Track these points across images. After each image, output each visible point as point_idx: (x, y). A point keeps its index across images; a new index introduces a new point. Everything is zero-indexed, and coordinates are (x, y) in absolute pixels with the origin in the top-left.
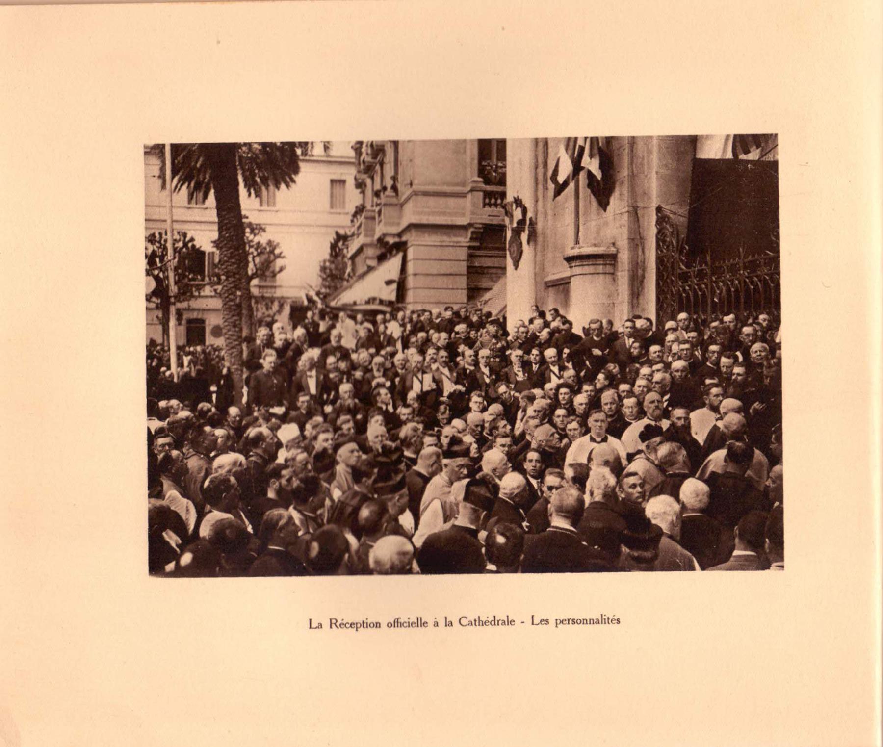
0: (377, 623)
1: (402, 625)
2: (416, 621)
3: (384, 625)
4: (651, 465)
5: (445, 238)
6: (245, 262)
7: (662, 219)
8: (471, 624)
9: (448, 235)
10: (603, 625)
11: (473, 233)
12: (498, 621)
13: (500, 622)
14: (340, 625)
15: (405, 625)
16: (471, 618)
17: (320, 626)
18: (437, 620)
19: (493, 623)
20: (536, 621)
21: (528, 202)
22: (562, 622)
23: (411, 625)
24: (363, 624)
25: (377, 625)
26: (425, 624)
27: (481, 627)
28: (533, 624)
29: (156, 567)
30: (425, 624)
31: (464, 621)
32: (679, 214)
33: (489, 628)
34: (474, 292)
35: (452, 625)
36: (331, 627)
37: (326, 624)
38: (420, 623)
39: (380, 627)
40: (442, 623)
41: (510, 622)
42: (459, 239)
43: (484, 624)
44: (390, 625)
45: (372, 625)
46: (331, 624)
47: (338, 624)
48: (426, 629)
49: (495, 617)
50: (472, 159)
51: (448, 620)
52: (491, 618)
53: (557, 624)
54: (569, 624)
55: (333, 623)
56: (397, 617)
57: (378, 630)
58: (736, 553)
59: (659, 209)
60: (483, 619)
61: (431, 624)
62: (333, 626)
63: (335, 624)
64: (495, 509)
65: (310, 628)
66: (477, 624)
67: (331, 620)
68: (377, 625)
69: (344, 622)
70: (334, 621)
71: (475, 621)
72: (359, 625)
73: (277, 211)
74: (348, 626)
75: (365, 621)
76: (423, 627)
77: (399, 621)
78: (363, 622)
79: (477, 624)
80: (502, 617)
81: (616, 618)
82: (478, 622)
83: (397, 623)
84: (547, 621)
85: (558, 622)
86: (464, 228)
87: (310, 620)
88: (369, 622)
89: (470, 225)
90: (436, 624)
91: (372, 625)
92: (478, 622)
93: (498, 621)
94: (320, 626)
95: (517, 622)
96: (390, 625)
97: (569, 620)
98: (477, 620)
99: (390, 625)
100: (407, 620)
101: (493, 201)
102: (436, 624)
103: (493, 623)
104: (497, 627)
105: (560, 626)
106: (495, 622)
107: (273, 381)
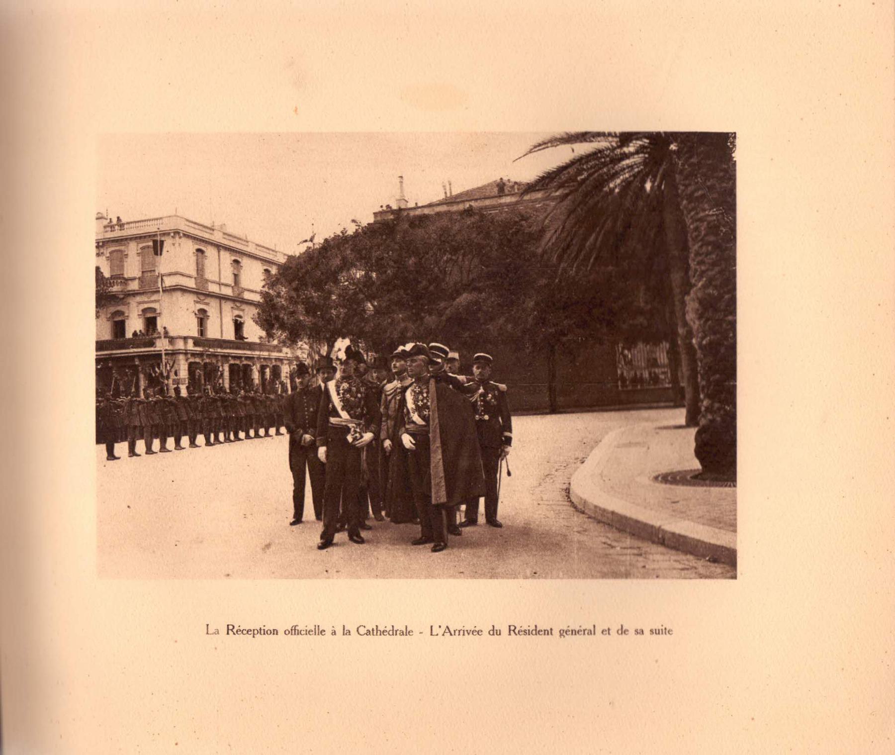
0: (575, 634)
1: (299, 633)
3: (281, 632)
8: (368, 633)
12: (396, 631)
13: (398, 632)
14: (519, 632)
15: (302, 632)
17: (217, 632)
22: (590, 633)
23: (308, 632)
24: (260, 631)
25: (275, 632)
26: (322, 632)
28: (431, 635)
29: (735, 133)
30: (322, 632)
31: (362, 631)
33: (387, 638)
36: (228, 634)
37: (505, 631)
40: (339, 631)
41: (407, 632)
43: (383, 633)
45: (269, 632)
47: (517, 631)
48: (628, 636)
49: (536, 626)
50: (647, 420)
52: (389, 628)
54: (584, 634)
55: (512, 630)
60: (381, 628)
63: (514, 631)
65: (431, 635)
66: (375, 633)
67: (510, 626)
68: (275, 632)
70: (512, 628)
71: (373, 630)
72: (256, 632)
73: (450, 184)
74: (245, 632)
77: (297, 628)
78: (260, 629)
79: (375, 633)
80: (400, 627)
82: (376, 631)
83: (294, 631)
84: (637, 632)
87: (208, 625)
90: (334, 633)
91: (269, 632)
92: (376, 631)
93: (396, 631)
94: (217, 632)
95: (416, 633)
96: (287, 632)
97: (584, 631)
98: (375, 629)
100: (527, 628)
103: (391, 633)
106: (394, 632)
107: (378, 277)
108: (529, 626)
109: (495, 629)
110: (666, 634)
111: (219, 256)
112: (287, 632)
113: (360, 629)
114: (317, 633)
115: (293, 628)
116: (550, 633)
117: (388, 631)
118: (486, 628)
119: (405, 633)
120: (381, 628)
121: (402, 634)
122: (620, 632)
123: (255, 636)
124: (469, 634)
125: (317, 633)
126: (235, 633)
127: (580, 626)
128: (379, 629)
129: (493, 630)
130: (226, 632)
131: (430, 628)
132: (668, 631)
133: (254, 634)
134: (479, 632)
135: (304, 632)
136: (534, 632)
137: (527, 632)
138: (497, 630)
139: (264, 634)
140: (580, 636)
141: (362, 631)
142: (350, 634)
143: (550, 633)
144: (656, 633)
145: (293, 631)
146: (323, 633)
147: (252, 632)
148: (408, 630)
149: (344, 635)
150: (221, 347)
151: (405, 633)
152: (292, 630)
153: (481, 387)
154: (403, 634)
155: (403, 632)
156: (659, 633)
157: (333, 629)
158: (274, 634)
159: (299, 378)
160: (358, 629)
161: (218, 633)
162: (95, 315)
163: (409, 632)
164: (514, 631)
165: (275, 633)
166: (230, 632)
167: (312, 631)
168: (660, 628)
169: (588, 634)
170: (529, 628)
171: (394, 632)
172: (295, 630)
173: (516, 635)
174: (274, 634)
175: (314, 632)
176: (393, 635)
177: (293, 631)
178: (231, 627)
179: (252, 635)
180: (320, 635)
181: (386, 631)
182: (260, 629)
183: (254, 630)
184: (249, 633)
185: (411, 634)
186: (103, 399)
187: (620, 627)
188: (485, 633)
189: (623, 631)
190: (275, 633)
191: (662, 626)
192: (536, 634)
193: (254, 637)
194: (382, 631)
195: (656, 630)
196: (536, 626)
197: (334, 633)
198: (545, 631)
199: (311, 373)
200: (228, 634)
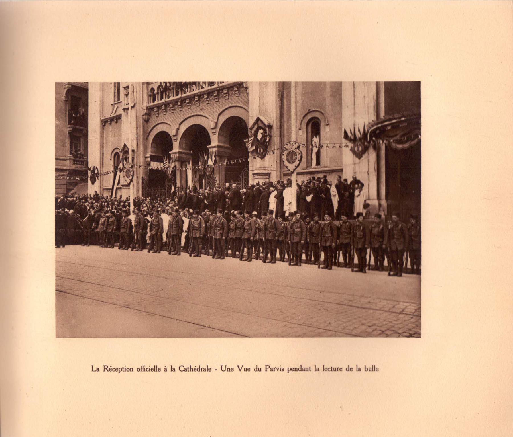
3: (135, 370)
5: (60, 173)
6: (146, 221)
7: (143, 179)
8: (186, 370)
9: (61, 172)
10: (307, 372)
11: (69, 172)
12: (202, 369)
13: (203, 369)
14: (110, 369)
15: (147, 370)
17: (98, 370)
19: (198, 370)
20: (95, 369)
21: (99, 169)
22: (291, 369)
23: (151, 370)
25: (131, 370)
26: (159, 370)
27: (191, 372)
30: (159, 370)
32: (146, 178)
35: (360, 370)
36: (104, 371)
37: (101, 369)
38: (156, 369)
39: (133, 371)
40: (169, 369)
41: (209, 370)
42: (65, 173)
43: (194, 370)
44: (138, 370)
46: (104, 368)
47: (108, 369)
50: (68, 149)
51: (172, 368)
52: (197, 367)
57: (360, 372)
59: (142, 177)
60: (193, 367)
61: (163, 369)
62: (106, 370)
63: (107, 369)
65: (92, 371)
68: (131, 370)
69: (112, 368)
71: (188, 368)
75: (124, 367)
76: (209, 372)
77: (144, 367)
78: (123, 368)
80: (204, 366)
81: (281, 367)
82: (190, 369)
83: (142, 369)
85: (289, 369)
86: (66, 170)
87: (92, 366)
89: (69, 169)
90: (166, 370)
92: (190, 369)
94: (98, 370)
95: (213, 370)
96: (138, 370)
98: (189, 367)
99: (138, 370)
100: (149, 367)
101: (75, 162)
102: (317, 370)
103: (198, 370)
104: (200, 372)
105: (291, 372)
106: (200, 369)
108: (150, 366)
109: (302, 367)
110: (246, 368)
112: (138, 370)
113: (181, 367)
114: (156, 370)
115: (142, 367)
116: (309, 370)
117: (112, 368)
118: (345, 367)
119: (206, 370)
121: (205, 370)
122: (348, 369)
123: (289, 372)
124: (278, 370)
125: (156, 370)
126: (109, 370)
127: (280, 366)
128: (366, 367)
129: (200, 368)
130: (265, 370)
131: (323, 366)
132: (375, 369)
133: (119, 371)
134: (341, 369)
135: (149, 370)
136: (300, 369)
137: (281, 370)
138: (259, 368)
139: (125, 371)
140: (326, 372)
143: (309, 370)
144: (369, 370)
145: (142, 369)
146: (159, 370)
147: (118, 370)
148: (208, 368)
150: (287, 105)
151: (206, 370)
152: (141, 368)
154: (205, 371)
155: (205, 369)
156: (371, 370)
157: (165, 368)
158: (141, 371)
161: (319, 370)
162: (366, 80)
163: (376, 369)
165: (132, 370)
166: (105, 370)
167: (153, 369)
169: (204, 370)
171: (200, 369)
172: (143, 368)
173: (108, 371)
174: (141, 371)
175: (154, 370)
176: (257, 371)
177: (142, 369)
178: (106, 367)
179: (118, 372)
180: (158, 371)
181: (111, 369)
182: (123, 368)
183: (119, 369)
184: (117, 370)
185: (351, 370)
186: (316, 187)
188: (344, 369)
189: (349, 369)
190: (132, 370)
191: (125, 366)
192: (349, 370)
193: (119, 372)
194: (146, 369)
195: (369, 368)
197: (166, 370)
198: (295, 368)
200: (104, 371)
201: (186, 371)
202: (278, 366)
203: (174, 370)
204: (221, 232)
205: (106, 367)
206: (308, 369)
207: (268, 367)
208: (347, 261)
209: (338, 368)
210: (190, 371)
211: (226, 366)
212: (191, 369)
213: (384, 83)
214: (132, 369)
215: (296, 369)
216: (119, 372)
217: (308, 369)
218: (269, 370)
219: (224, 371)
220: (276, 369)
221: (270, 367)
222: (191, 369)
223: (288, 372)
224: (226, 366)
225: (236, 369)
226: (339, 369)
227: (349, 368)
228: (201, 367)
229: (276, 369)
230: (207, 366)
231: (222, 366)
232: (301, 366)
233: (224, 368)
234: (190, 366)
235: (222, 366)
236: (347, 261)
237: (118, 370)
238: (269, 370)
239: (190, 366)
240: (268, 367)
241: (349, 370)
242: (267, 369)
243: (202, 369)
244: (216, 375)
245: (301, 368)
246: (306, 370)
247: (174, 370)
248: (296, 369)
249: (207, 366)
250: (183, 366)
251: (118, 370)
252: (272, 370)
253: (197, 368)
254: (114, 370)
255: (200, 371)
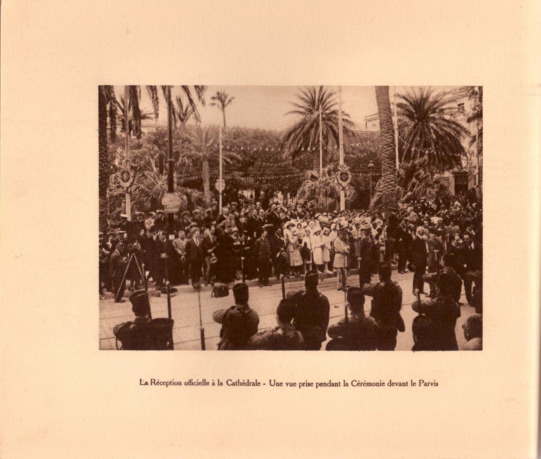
1: (193, 384)
2: (202, 382)
3: (183, 384)
4: (222, 125)
8: (234, 384)
12: (250, 383)
13: (251, 384)
14: (157, 383)
15: (195, 384)
16: (234, 381)
18: (214, 382)
19: (247, 384)
20: (143, 383)
22: (303, 384)
23: (199, 384)
24: (170, 383)
25: (180, 384)
34: (19, 257)
35: (222, 385)
38: (205, 383)
40: (216, 383)
41: (257, 384)
43: (242, 384)
44: (186, 384)
46: (151, 382)
47: (156, 383)
49: (248, 380)
52: (246, 381)
53: (300, 386)
56: (191, 379)
58: (304, 275)
60: (241, 381)
62: (153, 384)
63: (154, 382)
64: (453, 135)
65: (141, 384)
66: (237, 384)
68: (180, 384)
69: (159, 381)
71: (236, 382)
72: (168, 383)
75: (172, 381)
76: (382, 386)
77: (192, 381)
78: (171, 382)
79: (237, 384)
81: (436, 382)
83: (190, 383)
85: (301, 385)
88: (174, 381)
94: (147, 383)
95: (262, 384)
96: (186, 384)
97: (361, 383)
98: (237, 381)
99: (186, 384)
103: (247, 384)
106: (248, 384)
111: (415, 94)
120: (241, 381)
121: (254, 384)
122: (389, 384)
124: (432, 385)
128: (240, 381)
129: (248, 383)
133: (167, 385)
135: (197, 384)
136: (329, 385)
141: (354, 383)
142: (348, 386)
148: (258, 382)
149: (218, 385)
153: (407, 261)
155: (254, 383)
159: (420, 212)
160: (227, 382)
164: (154, 382)
166: (153, 383)
168: (379, 382)
170: (434, 382)
171: (248, 384)
173: (155, 385)
178: (153, 381)
182: (171, 382)
187: (390, 382)
188: (386, 384)
193: (167, 386)
196: (248, 380)
199: (338, 226)
201: (234, 385)
202: (432, 381)
203: (222, 384)
204: (298, 218)
205: (153, 381)
206: (337, 385)
207: (422, 382)
208: (448, 241)
209: (428, 383)
210: (239, 385)
211: (275, 380)
212: (240, 384)
213: (129, 87)
214: (185, 384)
215: (325, 385)
216: (167, 386)
217: (337, 385)
218: (422, 385)
219: (273, 386)
220: (430, 384)
221: (425, 382)
222: (240, 384)
223: (317, 388)
224: (275, 380)
225: (284, 385)
226: (362, 384)
227: (248, 383)
228: (250, 381)
229: (430, 384)
230: (256, 380)
231: (270, 381)
232: (391, 381)
233: (272, 383)
234: (239, 380)
235: (270, 381)
236: (448, 241)
237: (167, 384)
238: (422, 385)
239: (239, 380)
240: (422, 382)
241: (391, 386)
242: (421, 384)
243: (250, 383)
244: (265, 390)
245: (330, 383)
246: (236, 385)
247: (222, 384)
248: (325, 385)
249: (256, 380)
250: (231, 380)
251: (167, 384)
252: (426, 385)
253: (245, 382)
254: (161, 384)
255: (248, 385)
